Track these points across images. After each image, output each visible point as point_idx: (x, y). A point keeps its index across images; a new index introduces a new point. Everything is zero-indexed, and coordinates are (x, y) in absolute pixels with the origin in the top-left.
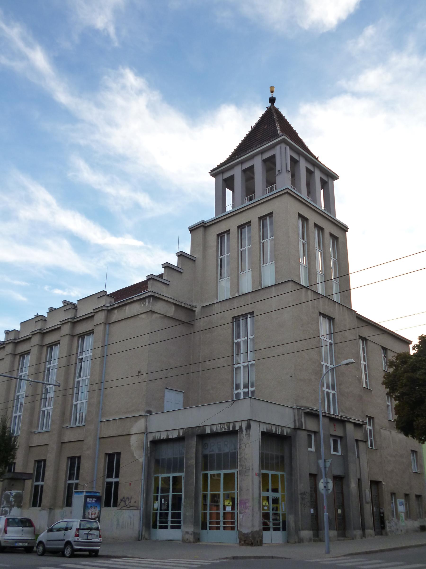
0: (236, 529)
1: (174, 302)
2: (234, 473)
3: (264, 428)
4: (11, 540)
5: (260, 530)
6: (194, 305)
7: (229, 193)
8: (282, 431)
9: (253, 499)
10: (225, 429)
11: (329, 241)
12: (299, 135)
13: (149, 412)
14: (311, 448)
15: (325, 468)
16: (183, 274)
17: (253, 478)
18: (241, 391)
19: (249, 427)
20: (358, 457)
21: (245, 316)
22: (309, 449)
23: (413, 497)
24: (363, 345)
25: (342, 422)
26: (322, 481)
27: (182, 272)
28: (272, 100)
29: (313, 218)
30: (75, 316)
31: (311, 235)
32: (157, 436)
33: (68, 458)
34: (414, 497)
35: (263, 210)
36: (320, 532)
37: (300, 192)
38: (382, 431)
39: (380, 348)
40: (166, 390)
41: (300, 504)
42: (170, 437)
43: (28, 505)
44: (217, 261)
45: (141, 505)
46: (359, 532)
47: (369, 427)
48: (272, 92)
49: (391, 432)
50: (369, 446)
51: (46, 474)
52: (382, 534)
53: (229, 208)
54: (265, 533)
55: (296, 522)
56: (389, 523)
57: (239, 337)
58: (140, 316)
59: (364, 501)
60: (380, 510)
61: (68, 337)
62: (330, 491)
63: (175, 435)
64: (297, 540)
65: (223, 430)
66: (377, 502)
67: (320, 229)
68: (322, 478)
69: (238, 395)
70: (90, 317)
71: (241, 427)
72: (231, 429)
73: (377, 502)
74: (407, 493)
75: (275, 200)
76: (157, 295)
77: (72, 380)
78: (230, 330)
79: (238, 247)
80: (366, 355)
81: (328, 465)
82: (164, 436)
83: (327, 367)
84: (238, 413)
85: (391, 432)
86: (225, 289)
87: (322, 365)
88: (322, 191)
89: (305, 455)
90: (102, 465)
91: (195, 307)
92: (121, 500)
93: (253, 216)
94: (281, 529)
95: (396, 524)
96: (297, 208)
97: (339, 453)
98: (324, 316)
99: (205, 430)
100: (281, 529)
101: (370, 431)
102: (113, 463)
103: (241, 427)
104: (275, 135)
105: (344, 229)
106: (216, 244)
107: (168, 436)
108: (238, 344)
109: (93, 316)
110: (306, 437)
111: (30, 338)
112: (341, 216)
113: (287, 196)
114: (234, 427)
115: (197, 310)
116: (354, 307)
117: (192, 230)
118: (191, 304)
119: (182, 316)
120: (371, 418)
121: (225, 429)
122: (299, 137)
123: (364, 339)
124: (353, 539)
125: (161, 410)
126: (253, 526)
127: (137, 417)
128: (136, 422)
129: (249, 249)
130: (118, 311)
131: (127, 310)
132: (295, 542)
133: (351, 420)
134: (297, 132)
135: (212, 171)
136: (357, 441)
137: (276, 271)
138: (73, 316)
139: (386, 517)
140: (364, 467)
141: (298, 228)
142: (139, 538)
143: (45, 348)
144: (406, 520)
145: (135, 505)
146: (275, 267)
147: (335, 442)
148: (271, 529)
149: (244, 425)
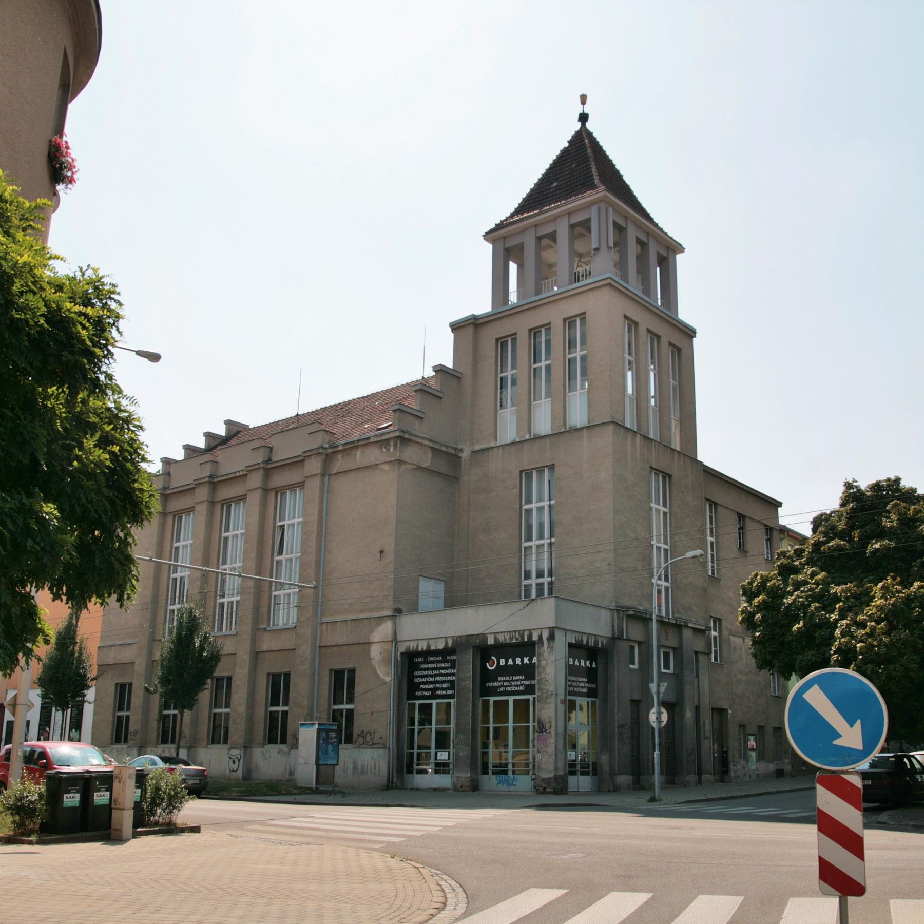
0: (531, 773)
1: (431, 444)
2: (528, 700)
3: (572, 639)
4: (651, 762)
6: (460, 447)
7: (513, 267)
8: (596, 642)
9: (557, 734)
10: (517, 639)
11: (666, 351)
12: (625, 178)
13: (399, 611)
14: (634, 664)
15: (658, 693)
17: (556, 706)
18: (534, 581)
19: (552, 637)
20: (697, 676)
21: (540, 470)
22: (631, 666)
24: (711, 512)
25: (679, 627)
26: (654, 710)
28: (583, 118)
29: (645, 321)
30: (269, 460)
32: (412, 646)
33: (268, 674)
34: (771, 730)
35: (571, 308)
37: (627, 281)
38: (731, 637)
39: (736, 515)
40: (421, 579)
42: (433, 648)
43: (205, 742)
45: (391, 744)
46: (693, 778)
47: (714, 633)
49: (744, 639)
50: (713, 660)
51: (133, 700)
52: (723, 781)
53: (513, 298)
54: (572, 779)
56: (734, 765)
57: (529, 501)
58: (380, 467)
61: (260, 491)
62: (663, 724)
63: (441, 646)
64: (611, 788)
65: (514, 641)
66: (721, 736)
67: (655, 337)
68: (653, 706)
69: (528, 588)
70: (298, 462)
71: (540, 637)
72: (526, 640)
73: (721, 736)
76: (407, 436)
77: (269, 559)
78: (516, 491)
81: (662, 689)
82: (423, 646)
84: (539, 617)
85: (744, 639)
86: (509, 431)
87: (652, 545)
88: (658, 269)
89: (625, 671)
90: (326, 687)
91: (461, 450)
92: (359, 735)
93: (555, 315)
95: (744, 767)
96: (623, 307)
97: (671, 671)
98: (657, 471)
99: (486, 639)
101: (715, 638)
102: (343, 683)
103: (540, 637)
104: (589, 185)
105: (689, 333)
106: (493, 354)
107: (429, 646)
108: (529, 511)
109: (303, 460)
110: (628, 649)
111: (194, 488)
112: (685, 314)
113: (607, 288)
114: (530, 636)
115: (465, 455)
116: (700, 457)
117: (456, 327)
118: (454, 446)
119: (442, 466)
120: (717, 621)
121: (517, 639)
122: (624, 182)
123: (714, 504)
125: (414, 608)
126: (556, 769)
127: (380, 619)
128: (379, 624)
130: (343, 457)
131: (358, 457)
133: (690, 625)
134: (622, 172)
135: (487, 233)
136: (696, 653)
137: (590, 406)
138: (266, 459)
139: (730, 758)
140: (707, 688)
141: (624, 333)
142: (389, 786)
143: (219, 507)
144: (757, 761)
145: (381, 742)
147: (666, 655)
148: (579, 773)
149: (545, 635)
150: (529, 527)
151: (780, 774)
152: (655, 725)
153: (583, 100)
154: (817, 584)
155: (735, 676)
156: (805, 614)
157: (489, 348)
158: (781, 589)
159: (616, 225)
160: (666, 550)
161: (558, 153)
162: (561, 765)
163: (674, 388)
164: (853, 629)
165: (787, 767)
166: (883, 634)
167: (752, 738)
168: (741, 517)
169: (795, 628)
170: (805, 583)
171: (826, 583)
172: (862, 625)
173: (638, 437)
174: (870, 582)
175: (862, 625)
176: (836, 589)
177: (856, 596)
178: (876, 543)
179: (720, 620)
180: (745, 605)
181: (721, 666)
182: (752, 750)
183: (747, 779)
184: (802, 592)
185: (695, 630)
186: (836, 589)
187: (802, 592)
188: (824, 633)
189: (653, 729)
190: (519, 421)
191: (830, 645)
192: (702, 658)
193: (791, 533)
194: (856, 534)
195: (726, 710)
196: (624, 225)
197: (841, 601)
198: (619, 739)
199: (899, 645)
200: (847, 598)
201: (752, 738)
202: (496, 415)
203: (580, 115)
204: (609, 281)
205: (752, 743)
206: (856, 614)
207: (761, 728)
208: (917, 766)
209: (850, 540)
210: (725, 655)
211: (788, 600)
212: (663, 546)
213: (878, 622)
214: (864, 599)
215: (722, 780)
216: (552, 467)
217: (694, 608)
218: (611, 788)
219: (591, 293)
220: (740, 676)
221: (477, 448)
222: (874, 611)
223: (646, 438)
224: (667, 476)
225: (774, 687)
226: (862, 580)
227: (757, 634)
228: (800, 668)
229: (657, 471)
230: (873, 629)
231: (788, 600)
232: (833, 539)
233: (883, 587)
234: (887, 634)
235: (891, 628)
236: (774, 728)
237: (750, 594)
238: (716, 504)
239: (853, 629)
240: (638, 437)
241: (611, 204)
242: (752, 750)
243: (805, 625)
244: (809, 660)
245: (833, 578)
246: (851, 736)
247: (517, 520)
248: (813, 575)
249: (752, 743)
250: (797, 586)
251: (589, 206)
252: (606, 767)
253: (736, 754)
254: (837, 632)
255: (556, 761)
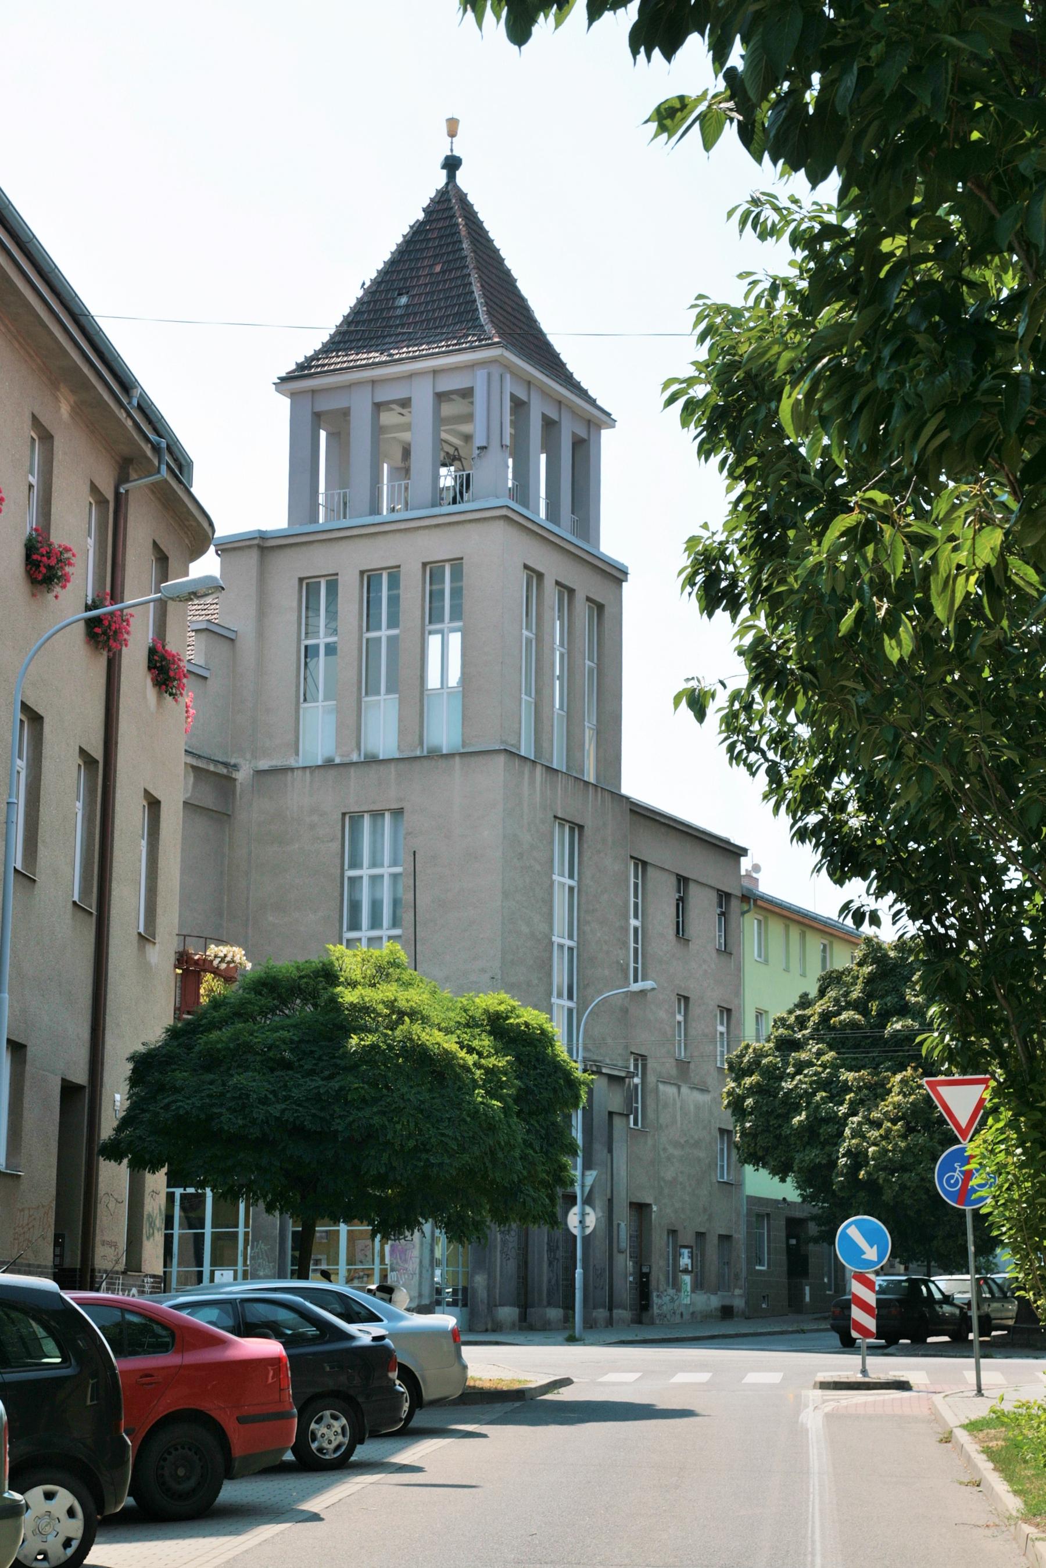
5: (431, 1303)
6: (233, 761)
11: (582, 608)
12: (519, 284)
16: (209, 682)
20: (610, 1151)
21: (377, 815)
23: (712, 1241)
24: (636, 877)
27: (205, 678)
28: (452, 164)
29: (554, 568)
31: (546, 617)
34: (715, 1241)
35: (438, 547)
36: (530, 1310)
38: (661, 1087)
41: (498, 1253)
44: (299, 651)
48: (452, 134)
49: (679, 1087)
50: (632, 1125)
55: (490, 1289)
56: (658, 1296)
57: (355, 864)
59: (615, 1250)
60: (641, 1269)
64: (489, 1327)
74: (702, 1230)
75: (468, 526)
78: (336, 846)
79: (361, 627)
80: (640, 901)
83: (561, 946)
85: (679, 1087)
86: (319, 737)
91: (236, 767)
94: (460, 1303)
95: (672, 1300)
98: (561, 820)
100: (460, 1303)
105: (615, 575)
106: (295, 604)
108: (354, 881)
112: (611, 544)
113: (501, 523)
115: (242, 776)
118: (224, 760)
119: (208, 799)
124: (591, 1327)
126: (420, 1295)
129: (390, 639)
132: (487, 1330)
133: (604, 1071)
135: (283, 379)
136: (611, 1114)
144: (693, 1291)
146: (463, 706)
150: (355, 907)
151: (727, 1312)
152: (576, 1232)
153: (452, 128)
154: (824, 1066)
155: (665, 1149)
156: (809, 1103)
157: (286, 597)
158: (779, 1068)
159: (513, 397)
160: (571, 949)
161: (406, 230)
162: (426, 1291)
163: (591, 671)
164: (865, 1128)
165: (739, 1303)
166: (899, 1136)
167: (686, 1252)
168: (682, 881)
169: (796, 1120)
170: (810, 1064)
171: (835, 1067)
172: (877, 1124)
173: (539, 768)
174: (887, 1069)
175: (877, 1124)
176: (848, 1076)
177: (869, 1087)
178: (897, 1022)
179: (644, 1058)
180: (733, 1085)
181: (643, 1132)
182: (686, 1271)
183: (678, 1319)
184: (806, 1076)
185: (611, 1078)
186: (848, 1076)
187: (806, 1076)
188: (831, 1129)
189: (575, 1237)
190: (340, 726)
191: (837, 1145)
192: (617, 1122)
193: (759, 903)
194: (874, 1006)
195: (649, 1205)
196: (524, 398)
197: (851, 1091)
198: (502, 1252)
199: (916, 1151)
200: (860, 1088)
201: (686, 1252)
202: (297, 711)
203: (447, 158)
204: (504, 512)
205: (685, 1261)
206: (869, 1110)
207: (700, 1236)
208: (937, 1296)
209: (865, 1012)
210: (651, 1115)
211: (787, 1085)
212: (568, 943)
213: (894, 1122)
214: (878, 1091)
215: (638, 1321)
216: (398, 813)
217: (609, 1041)
218: (489, 1327)
219: (473, 526)
220: (671, 1150)
221: (264, 764)
222: (890, 1108)
223: (549, 769)
224: (577, 828)
225: (722, 1167)
226: (878, 1065)
227: (748, 1125)
228: (799, 1168)
229: (561, 820)
230: (889, 1131)
231: (787, 1085)
232: (845, 1008)
233: (902, 1081)
234: (904, 1137)
235: (909, 1130)
236: (720, 1236)
237: (738, 1071)
238: (645, 864)
239: (865, 1128)
240: (539, 768)
241: (508, 367)
242: (686, 1271)
243: (807, 1118)
244: (811, 1161)
245: (842, 1059)
246: (871, 1254)
247: (337, 894)
248: (819, 1054)
249: (685, 1261)
250: (800, 1067)
251: (472, 366)
252: (482, 1294)
253: (662, 1278)
254: (847, 1132)
255: (420, 1284)
